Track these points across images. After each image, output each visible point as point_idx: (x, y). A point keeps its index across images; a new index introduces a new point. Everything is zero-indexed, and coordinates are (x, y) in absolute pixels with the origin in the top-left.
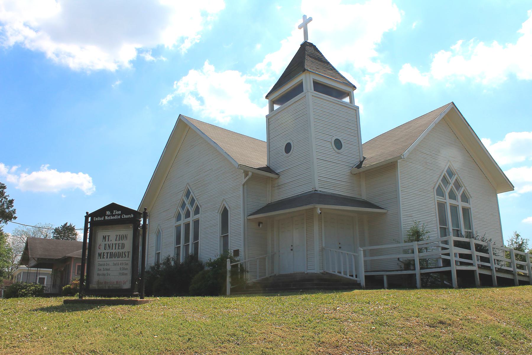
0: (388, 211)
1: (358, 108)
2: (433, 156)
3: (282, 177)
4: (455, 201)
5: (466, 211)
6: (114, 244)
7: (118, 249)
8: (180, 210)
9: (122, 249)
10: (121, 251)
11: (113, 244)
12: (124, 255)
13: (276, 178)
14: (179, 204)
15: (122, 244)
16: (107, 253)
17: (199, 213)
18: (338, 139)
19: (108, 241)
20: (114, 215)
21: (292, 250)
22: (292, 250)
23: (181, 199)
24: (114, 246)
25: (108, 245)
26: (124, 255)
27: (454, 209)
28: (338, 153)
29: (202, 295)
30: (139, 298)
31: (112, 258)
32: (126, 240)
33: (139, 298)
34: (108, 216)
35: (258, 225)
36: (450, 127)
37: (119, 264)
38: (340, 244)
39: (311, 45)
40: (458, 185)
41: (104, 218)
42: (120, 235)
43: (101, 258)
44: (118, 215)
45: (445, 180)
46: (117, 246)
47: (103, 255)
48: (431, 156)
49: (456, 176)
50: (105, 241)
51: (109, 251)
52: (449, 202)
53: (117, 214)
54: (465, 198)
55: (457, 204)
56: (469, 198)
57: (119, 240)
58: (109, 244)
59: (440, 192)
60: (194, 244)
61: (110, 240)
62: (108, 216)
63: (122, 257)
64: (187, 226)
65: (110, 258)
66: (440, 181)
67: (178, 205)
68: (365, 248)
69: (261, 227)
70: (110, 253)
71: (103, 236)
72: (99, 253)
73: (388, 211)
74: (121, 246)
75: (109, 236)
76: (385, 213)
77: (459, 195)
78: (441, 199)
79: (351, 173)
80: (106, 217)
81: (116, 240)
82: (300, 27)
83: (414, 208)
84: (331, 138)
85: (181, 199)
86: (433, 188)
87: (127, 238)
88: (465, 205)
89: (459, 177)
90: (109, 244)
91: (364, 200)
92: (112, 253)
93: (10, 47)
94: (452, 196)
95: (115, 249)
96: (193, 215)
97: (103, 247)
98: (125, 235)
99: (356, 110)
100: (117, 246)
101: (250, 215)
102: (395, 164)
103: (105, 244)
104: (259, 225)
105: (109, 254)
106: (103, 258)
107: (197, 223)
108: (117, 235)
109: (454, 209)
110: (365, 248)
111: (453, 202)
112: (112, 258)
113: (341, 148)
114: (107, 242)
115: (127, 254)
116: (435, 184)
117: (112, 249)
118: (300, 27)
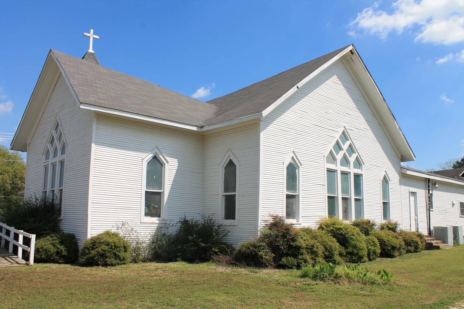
5: (358, 177)
8: (49, 148)
17: (65, 154)
29: (74, 241)
30: (23, 231)
33: (23, 231)
36: (48, 99)
40: (351, 149)
45: (338, 147)
54: (358, 163)
64: (54, 165)
77: (352, 159)
83: (317, 115)
88: (358, 171)
94: (345, 161)
107: (62, 163)
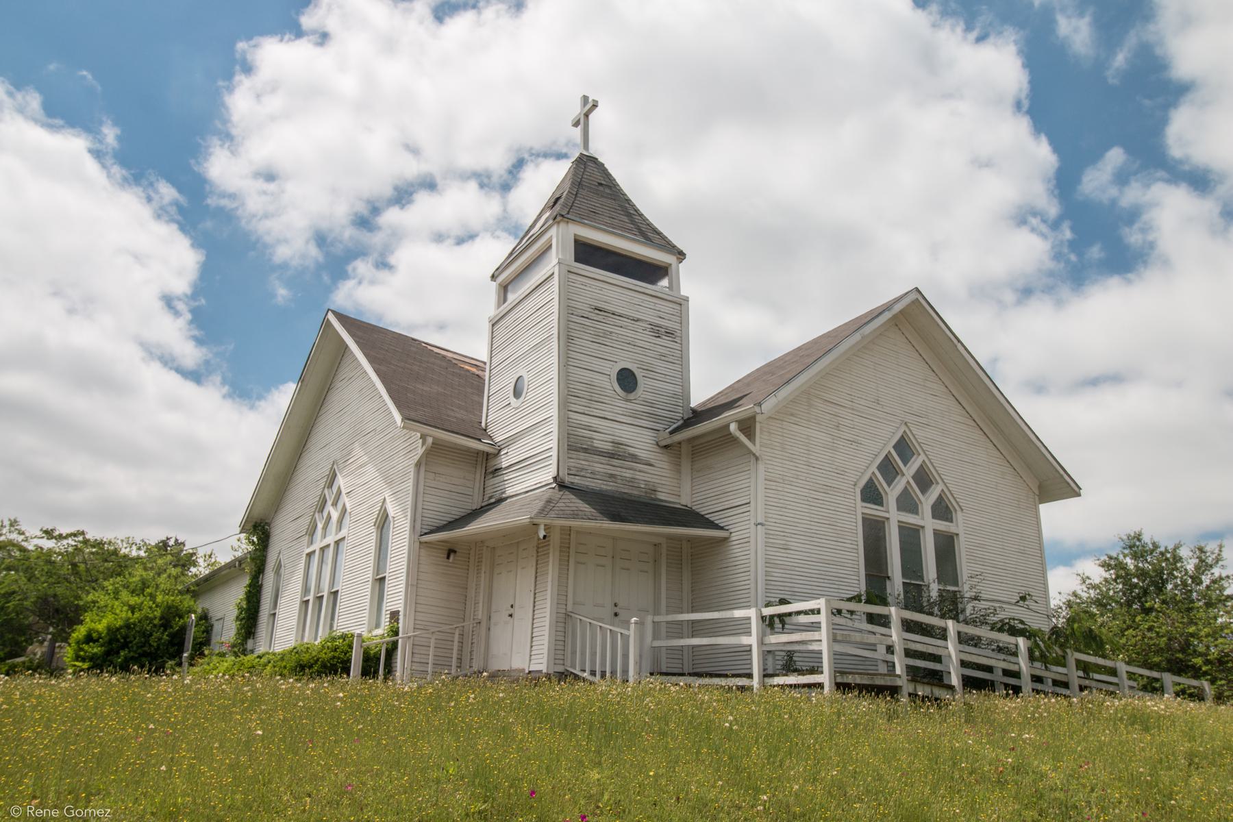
0: (731, 533)
1: (687, 299)
2: (863, 412)
4: (916, 516)
14: (317, 505)
21: (511, 616)
22: (511, 616)
27: (910, 536)
28: (627, 400)
35: (446, 556)
38: (616, 605)
39: (594, 160)
40: (924, 480)
45: (888, 469)
48: (853, 409)
49: (922, 457)
52: (894, 517)
54: (942, 510)
55: (921, 523)
56: (956, 510)
59: (871, 494)
66: (874, 468)
67: (316, 508)
68: (657, 619)
73: (731, 533)
76: (726, 539)
77: (927, 502)
78: (873, 510)
79: (658, 445)
82: (576, 124)
84: (611, 366)
86: (853, 483)
89: (929, 460)
91: (686, 506)
99: (681, 305)
101: (426, 534)
102: (750, 427)
104: (448, 557)
109: (910, 536)
110: (657, 619)
111: (910, 519)
113: (637, 383)
116: (860, 474)
118: (576, 124)
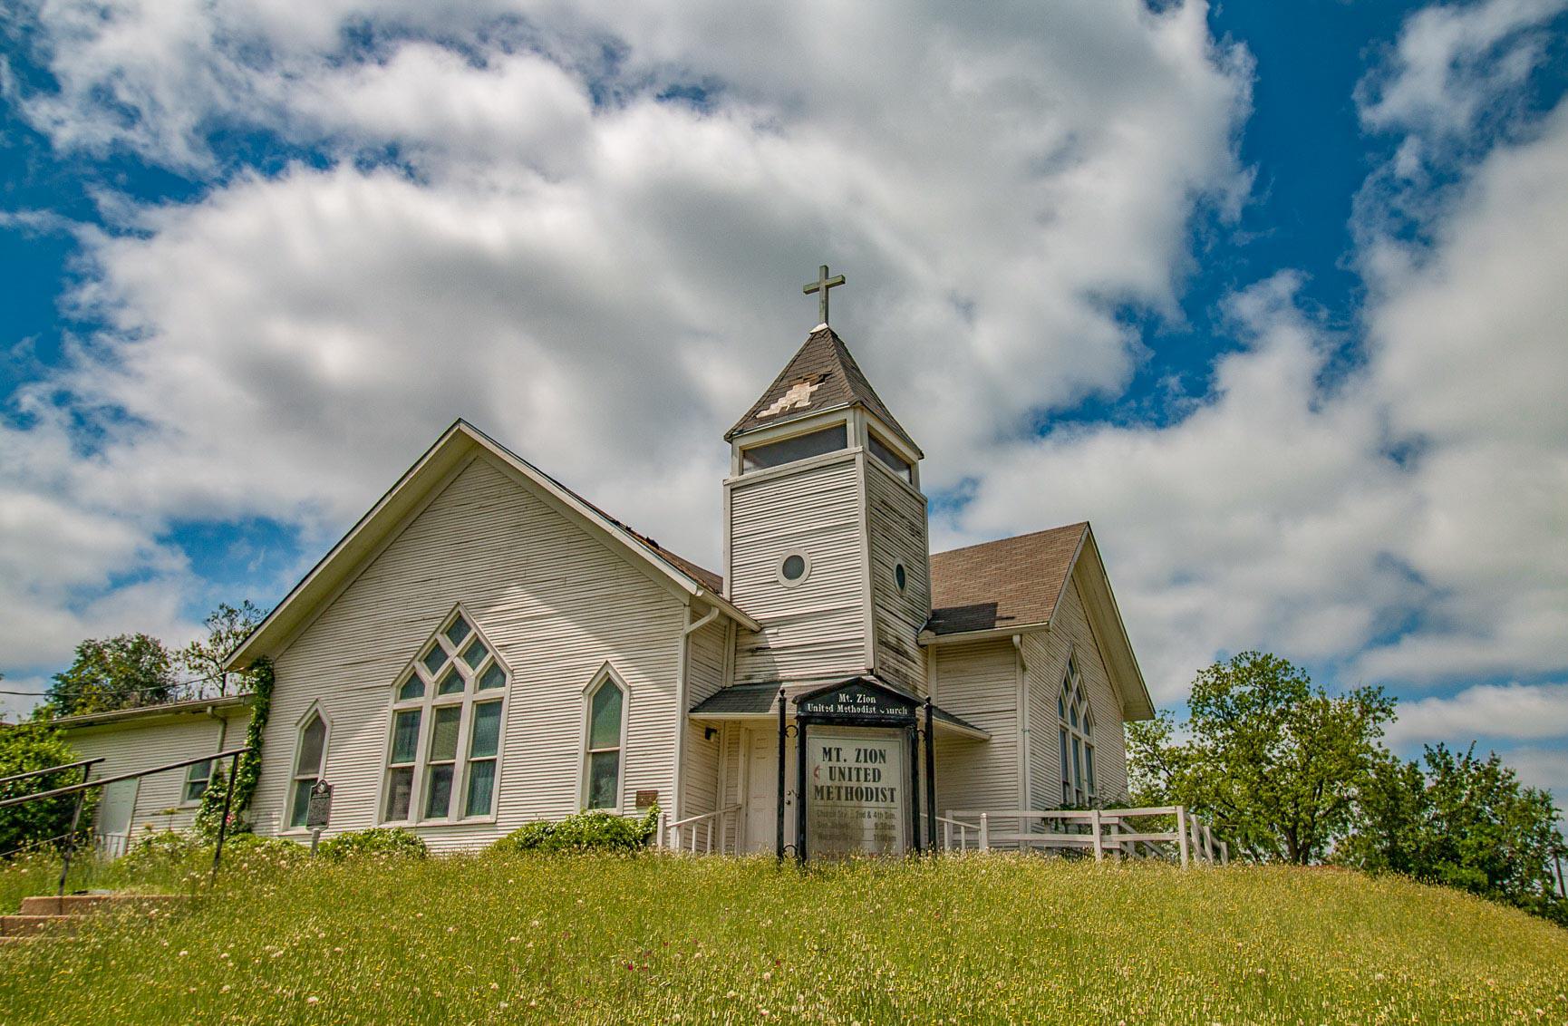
3: (767, 632)
6: (853, 770)
7: (866, 780)
9: (874, 781)
10: (872, 785)
11: (850, 769)
12: (880, 796)
13: (752, 631)
15: (874, 770)
16: (839, 788)
18: (789, 558)
19: (838, 760)
20: (861, 705)
23: (428, 640)
24: (854, 773)
25: (837, 769)
26: (880, 796)
31: (852, 799)
32: (882, 761)
34: (846, 704)
37: (872, 814)
41: (836, 708)
42: (866, 751)
43: (822, 798)
44: (870, 705)
46: (862, 773)
47: (829, 793)
50: (830, 760)
51: (846, 783)
53: (866, 704)
57: (866, 761)
58: (840, 768)
60: (470, 765)
61: (841, 759)
62: (846, 704)
63: (877, 800)
65: (847, 799)
69: (712, 740)
70: (847, 788)
71: (825, 749)
72: (816, 787)
74: (871, 774)
75: (838, 750)
80: (840, 708)
81: (857, 761)
85: (428, 640)
87: (884, 758)
90: (840, 768)
92: (852, 788)
93: (48, 55)
95: (858, 780)
96: (475, 688)
97: (824, 773)
98: (880, 751)
100: (862, 773)
103: (831, 768)
104: (708, 737)
105: (843, 792)
106: (828, 798)
108: (860, 750)
112: (852, 799)
114: (834, 763)
115: (888, 793)
117: (850, 780)
